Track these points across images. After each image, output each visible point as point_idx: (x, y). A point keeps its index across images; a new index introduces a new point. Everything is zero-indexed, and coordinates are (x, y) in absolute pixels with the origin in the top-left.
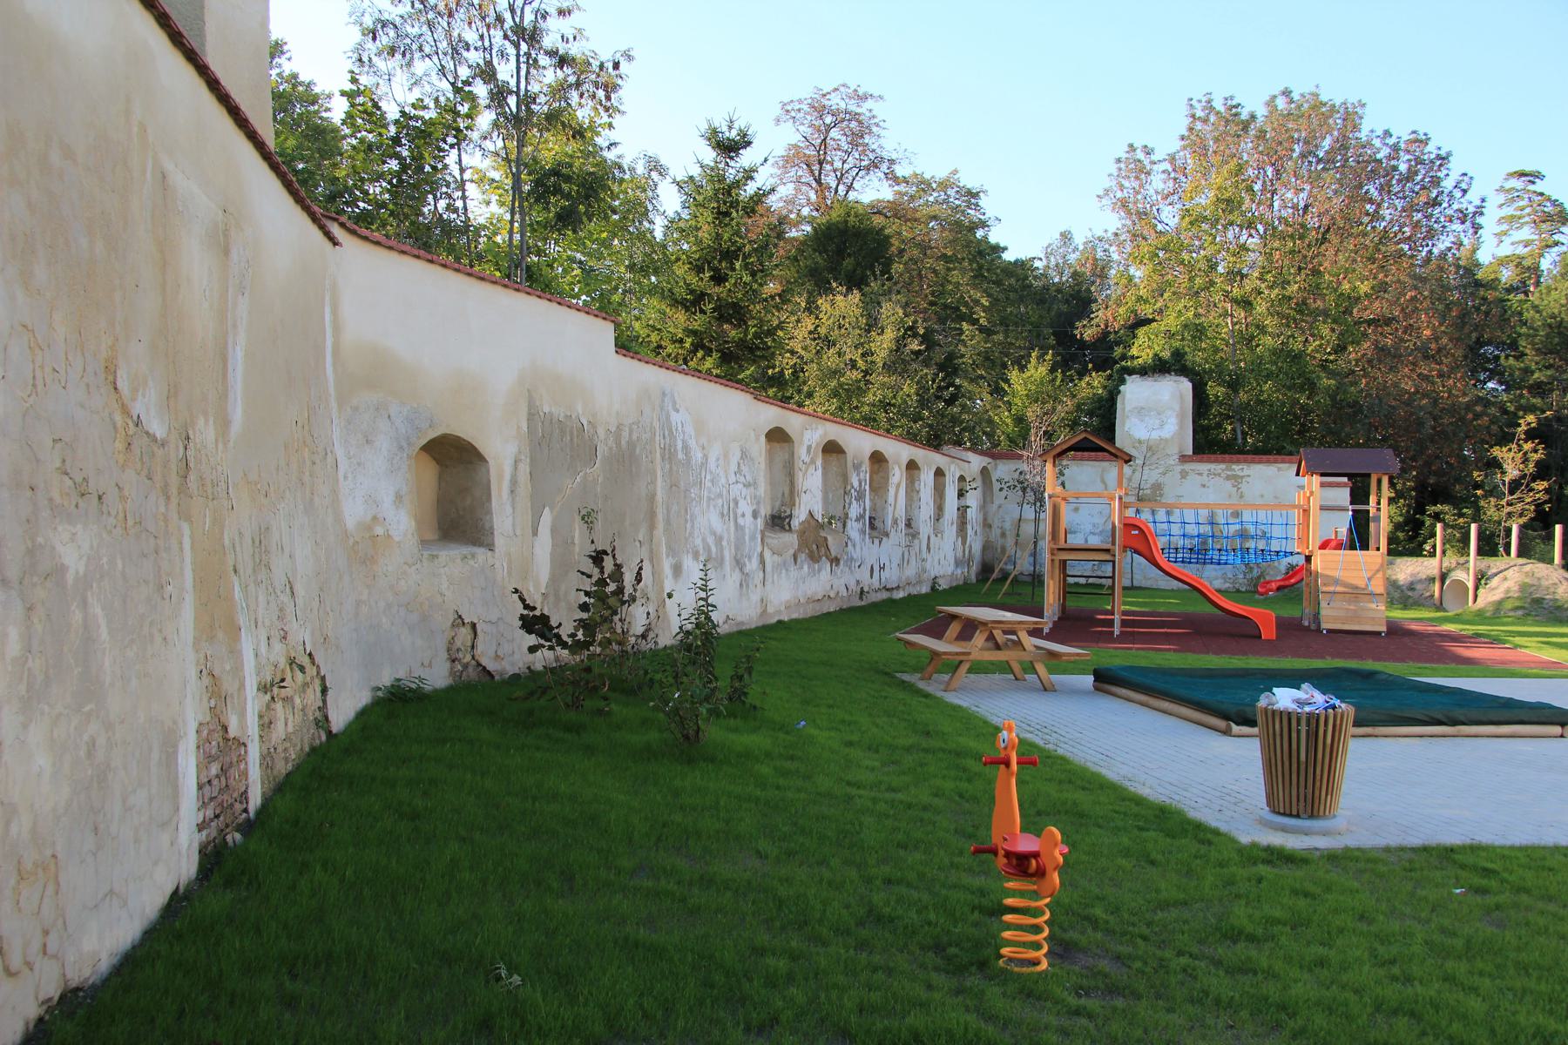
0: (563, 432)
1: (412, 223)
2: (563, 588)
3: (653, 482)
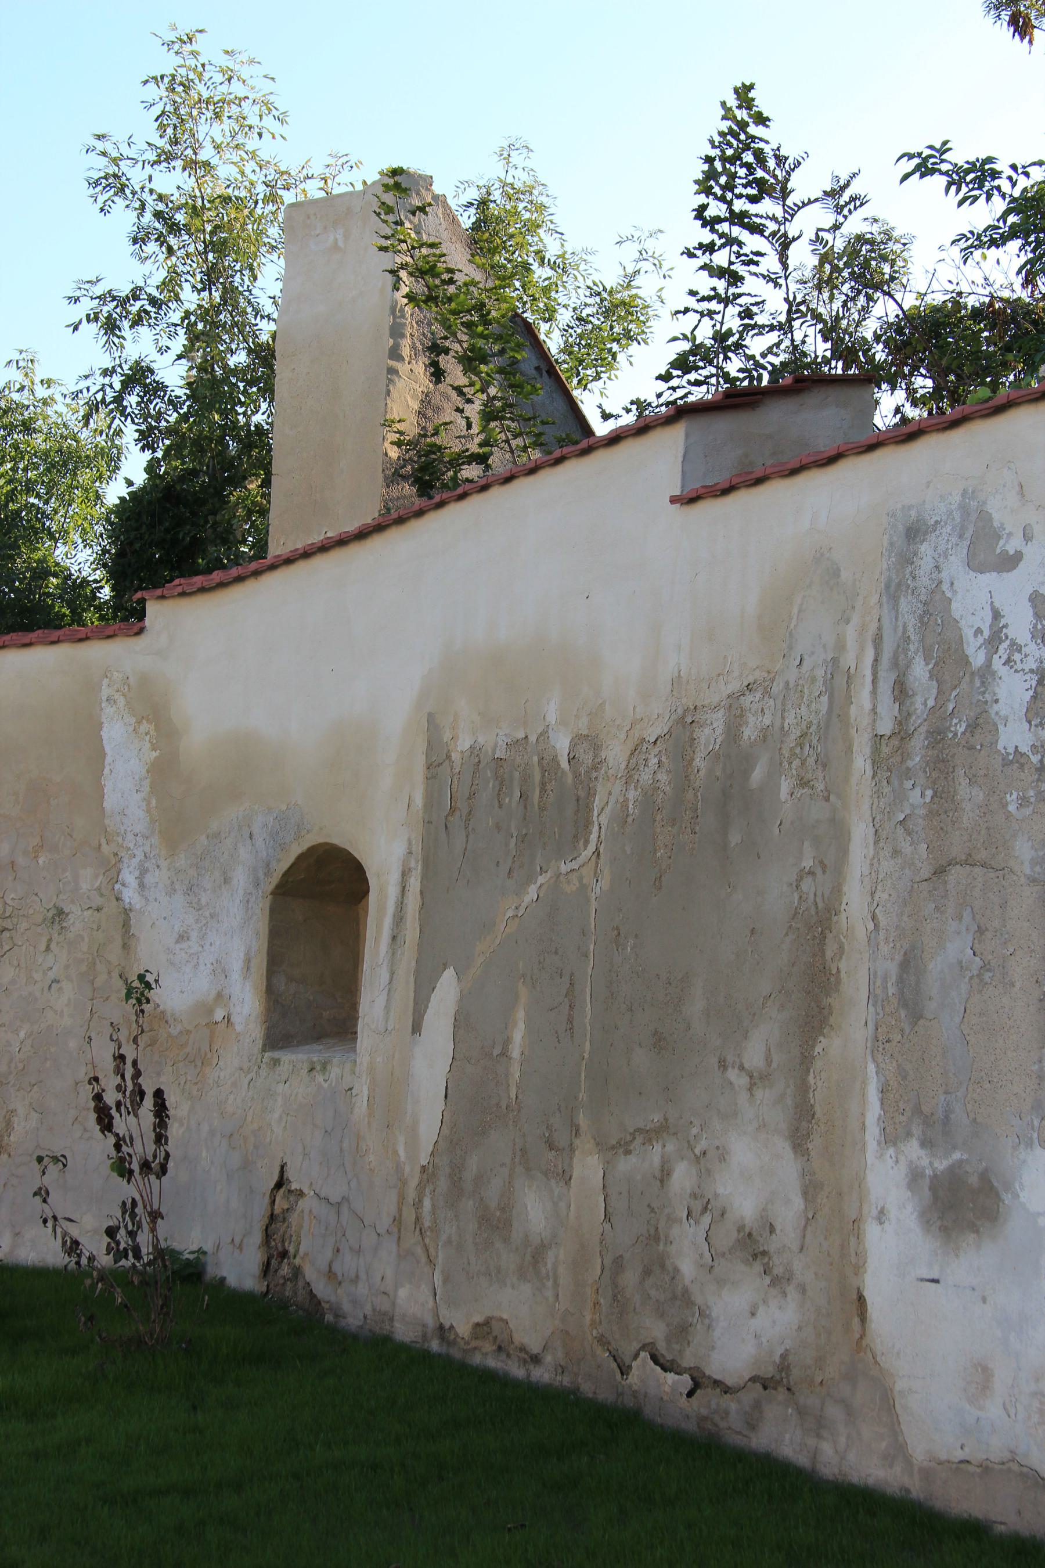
0: (502, 783)
1: (967, 358)
2: (473, 1164)
3: (832, 865)
